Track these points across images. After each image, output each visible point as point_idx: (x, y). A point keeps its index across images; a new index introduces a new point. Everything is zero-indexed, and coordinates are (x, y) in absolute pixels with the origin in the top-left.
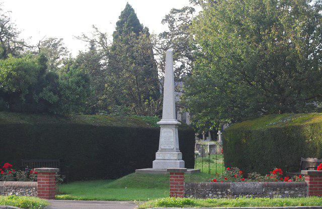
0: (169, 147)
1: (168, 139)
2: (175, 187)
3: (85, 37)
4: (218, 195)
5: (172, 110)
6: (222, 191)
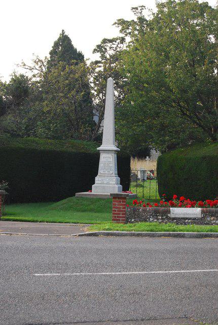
0: (104, 172)
1: (107, 163)
2: (119, 214)
3: (25, 65)
4: (158, 219)
5: (112, 137)
6: (162, 216)
